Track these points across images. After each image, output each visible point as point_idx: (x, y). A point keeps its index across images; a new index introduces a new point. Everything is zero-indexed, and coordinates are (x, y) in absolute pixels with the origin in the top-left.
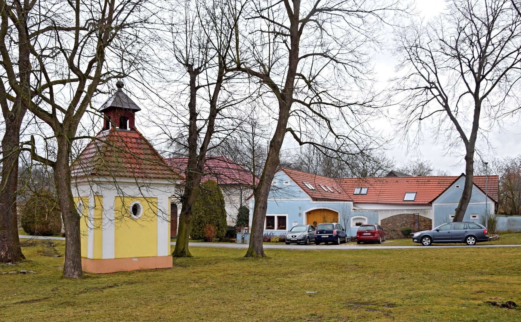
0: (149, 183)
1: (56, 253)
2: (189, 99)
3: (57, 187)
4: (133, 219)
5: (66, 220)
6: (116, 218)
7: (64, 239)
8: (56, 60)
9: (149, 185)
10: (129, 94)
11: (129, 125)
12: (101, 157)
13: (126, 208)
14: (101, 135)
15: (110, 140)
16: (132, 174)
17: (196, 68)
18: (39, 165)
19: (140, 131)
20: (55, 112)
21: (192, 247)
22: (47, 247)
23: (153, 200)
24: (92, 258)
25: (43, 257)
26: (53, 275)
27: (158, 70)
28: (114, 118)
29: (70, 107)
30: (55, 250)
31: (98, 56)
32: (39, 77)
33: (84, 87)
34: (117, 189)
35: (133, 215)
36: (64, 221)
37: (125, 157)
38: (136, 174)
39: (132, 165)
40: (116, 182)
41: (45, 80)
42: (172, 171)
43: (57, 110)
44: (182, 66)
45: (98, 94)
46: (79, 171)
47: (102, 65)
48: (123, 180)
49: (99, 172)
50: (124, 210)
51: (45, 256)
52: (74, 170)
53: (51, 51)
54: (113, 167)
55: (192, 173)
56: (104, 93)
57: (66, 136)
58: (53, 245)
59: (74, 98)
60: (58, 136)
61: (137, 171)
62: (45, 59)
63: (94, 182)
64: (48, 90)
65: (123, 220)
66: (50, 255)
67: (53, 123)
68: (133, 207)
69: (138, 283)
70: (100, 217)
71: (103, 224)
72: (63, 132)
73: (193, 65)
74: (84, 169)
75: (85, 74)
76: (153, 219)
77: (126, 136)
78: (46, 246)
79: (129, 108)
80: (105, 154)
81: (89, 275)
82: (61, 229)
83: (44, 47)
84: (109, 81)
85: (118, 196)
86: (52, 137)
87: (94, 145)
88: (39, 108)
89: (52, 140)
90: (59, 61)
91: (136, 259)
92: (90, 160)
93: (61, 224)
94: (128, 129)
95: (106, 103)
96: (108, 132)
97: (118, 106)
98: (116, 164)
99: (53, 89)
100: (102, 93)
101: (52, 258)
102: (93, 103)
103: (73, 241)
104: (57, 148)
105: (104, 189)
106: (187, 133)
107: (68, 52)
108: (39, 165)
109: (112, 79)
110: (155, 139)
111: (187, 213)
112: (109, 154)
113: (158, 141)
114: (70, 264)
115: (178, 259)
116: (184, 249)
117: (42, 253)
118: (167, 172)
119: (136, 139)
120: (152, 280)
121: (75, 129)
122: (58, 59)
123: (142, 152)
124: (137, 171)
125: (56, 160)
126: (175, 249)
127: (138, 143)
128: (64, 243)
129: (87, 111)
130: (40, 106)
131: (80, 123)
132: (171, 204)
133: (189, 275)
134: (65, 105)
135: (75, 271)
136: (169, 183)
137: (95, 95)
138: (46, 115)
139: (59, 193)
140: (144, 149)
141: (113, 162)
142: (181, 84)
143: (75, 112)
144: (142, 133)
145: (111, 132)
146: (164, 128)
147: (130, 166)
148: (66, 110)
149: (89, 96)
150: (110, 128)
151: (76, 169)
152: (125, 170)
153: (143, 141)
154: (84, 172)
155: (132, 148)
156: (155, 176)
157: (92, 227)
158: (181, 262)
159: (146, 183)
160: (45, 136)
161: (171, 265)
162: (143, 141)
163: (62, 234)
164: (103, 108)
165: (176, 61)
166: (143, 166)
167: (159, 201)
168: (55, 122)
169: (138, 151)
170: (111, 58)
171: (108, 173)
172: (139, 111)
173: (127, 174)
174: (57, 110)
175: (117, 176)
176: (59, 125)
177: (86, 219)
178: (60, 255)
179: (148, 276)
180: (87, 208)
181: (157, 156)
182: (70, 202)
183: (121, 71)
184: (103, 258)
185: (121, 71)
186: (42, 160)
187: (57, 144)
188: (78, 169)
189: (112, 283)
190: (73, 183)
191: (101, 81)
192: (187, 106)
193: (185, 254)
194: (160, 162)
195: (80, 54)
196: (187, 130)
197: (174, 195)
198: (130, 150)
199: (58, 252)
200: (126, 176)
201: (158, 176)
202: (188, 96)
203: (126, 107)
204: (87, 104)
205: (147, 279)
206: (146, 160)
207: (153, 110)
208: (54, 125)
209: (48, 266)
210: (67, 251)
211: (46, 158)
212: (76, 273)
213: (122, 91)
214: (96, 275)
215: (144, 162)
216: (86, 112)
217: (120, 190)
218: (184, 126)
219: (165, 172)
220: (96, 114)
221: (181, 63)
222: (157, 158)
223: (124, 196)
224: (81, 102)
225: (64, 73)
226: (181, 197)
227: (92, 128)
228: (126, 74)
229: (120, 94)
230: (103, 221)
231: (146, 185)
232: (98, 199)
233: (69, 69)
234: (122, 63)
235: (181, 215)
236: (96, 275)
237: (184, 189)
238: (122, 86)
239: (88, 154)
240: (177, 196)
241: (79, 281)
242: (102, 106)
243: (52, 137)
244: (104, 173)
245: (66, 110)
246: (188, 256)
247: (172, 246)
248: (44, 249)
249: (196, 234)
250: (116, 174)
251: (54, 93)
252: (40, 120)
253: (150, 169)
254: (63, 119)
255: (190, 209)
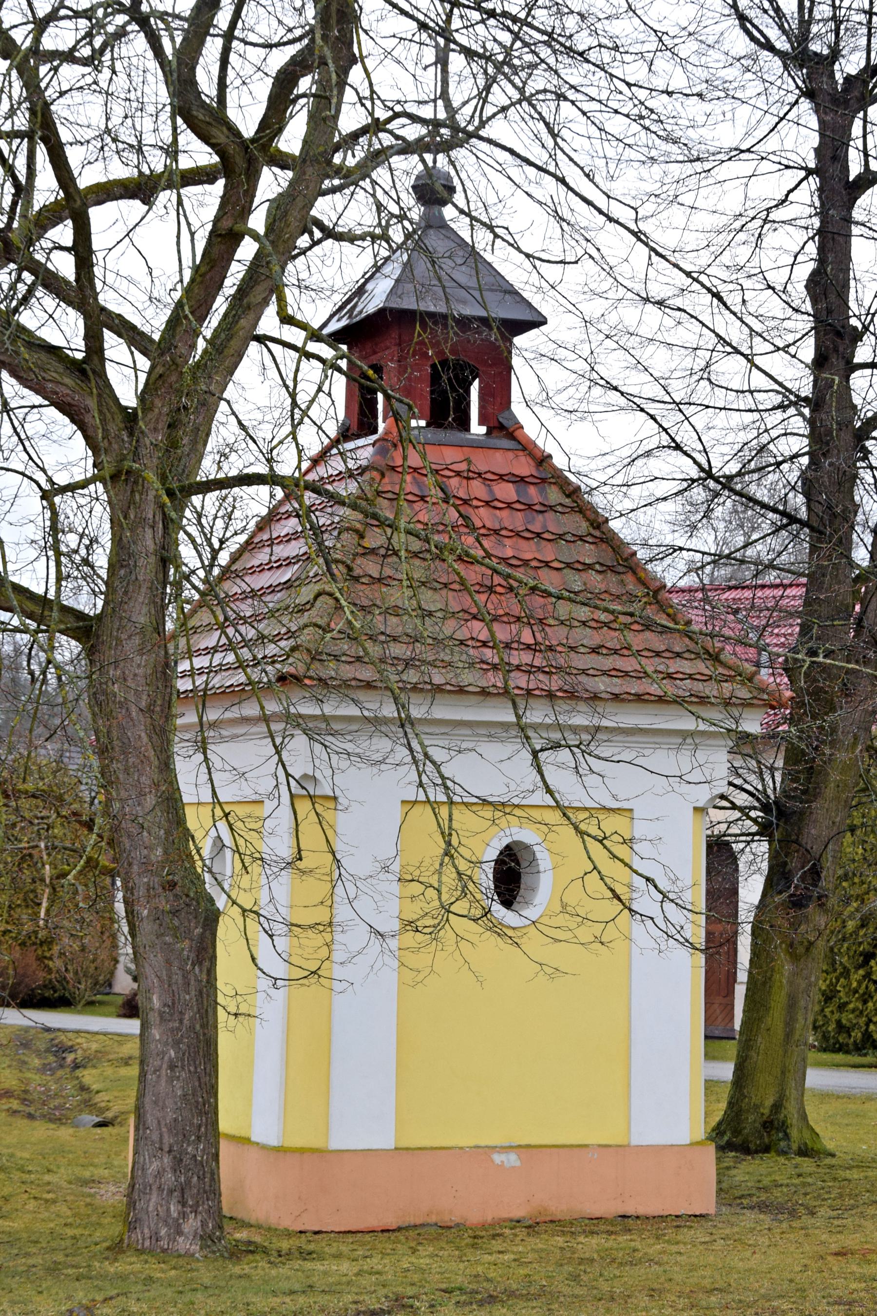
0: (586, 729)
1: (89, 1105)
2: (812, 249)
3: (103, 751)
4: (498, 929)
5: (147, 928)
6: (410, 925)
7: (133, 1026)
8: (106, 73)
9: (586, 737)
10: (482, 239)
11: (482, 408)
12: (332, 588)
13: (463, 866)
14: (336, 465)
15: (379, 493)
16: (495, 680)
17: (854, 72)
18: (16, 630)
19: (540, 443)
20: (101, 350)
21: (825, 1096)
22: (44, 1068)
23: (610, 824)
24: (273, 1142)
25: (22, 1123)
26: (70, 1232)
27: (642, 94)
28: (402, 370)
29: (173, 323)
30: (83, 1088)
31: (324, 37)
32: (21, 165)
33: (246, 211)
34: (415, 761)
35: (498, 910)
36: (133, 932)
37: (462, 582)
38: (519, 680)
39: (496, 626)
40: (412, 722)
41: (54, 184)
42: (715, 658)
43: (110, 338)
44: (773, 65)
45: (315, 243)
46: (218, 658)
47: (342, 83)
48: (443, 711)
49: (317, 670)
50: (449, 877)
51: (31, 1117)
52: (190, 654)
53: (83, 23)
54: (395, 639)
55: (824, 668)
56: (350, 238)
57: (151, 476)
58: (70, 1057)
59: (196, 269)
60: (115, 477)
61: (526, 658)
62: (56, 69)
63: (295, 721)
64: (63, 233)
65: (447, 934)
66: (58, 1119)
67: (88, 411)
68: (499, 862)
69: (527, 1297)
70: (322, 916)
71: (337, 956)
72: (136, 457)
73: (835, 53)
74: (245, 653)
75: (253, 140)
76: (610, 933)
77: (463, 467)
78: (36, 1062)
79: (483, 313)
80: (349, 569)
81: (258, 1239)
82: (112, 973)
83: (49, 9)
84: (381, 174)
85: (422, 797)
86: (84, 484)
87: (294, 521)
88: (23, 329)
89: (82, 501)
90: (121, 81)
91: (512, 1159)
92: (272, 600)
93: (115, 946)
94: (477, 429)
95: (360, 291)
96: (370, 449)
97: (423, 307)
98: (411, 624)
99: (94, 228)
100: (339, 237)
101: (64, 1133)
102: (290, 294)
103: (177, 1043)
104: (106, 539)
105: (344, 764)
106: (799, 444)
107: (168, 28)
108: (16, 630)
109: (396, 161)
110: (619, 480)
111: (798, 903)
112: (372, 567)
113: (635, 491)
114: (159, 1174)
115: (743, 1166)
116: (777, 1107)
117: (15, 1104)
118: (686, 667)
119: (519, 481)
120: (605, 1287)
121: (202, 434)
122: (118, 66)
123: (548, 552)
124: (526, 658)
125: (100, 603)
126: (730, 1104)
127: (530, 506)
128: (132, 1048)
129: (262, 339)
130: (27, 319)
131: (223, 406)
132: (709, 847)
133: (814, 1266)
134: (150, 312)
135: (184, 1215)
136: (702, 727)
137: (304, 252)
138: (54, 364)
139: (111, 783)
140: (561, 536)
141: (395, 611)
142: (766, 166)
143: (201, 344)
144: (550, 448)
145: (384, 446)
146: (670, 419)
147: (484, 636)
148: (156, 337)
149: (274, 259)
150: (381, 426)
151: (199, 653)
152: (458, 657)
153: (554, 495)
154: (241, 665)
155: (496, 532)
156: (617, 686)
157: (278, 969)
158: (766, 1181)
159: (575, 729)
160: (50, 480)
161: (707, 1203)
162: (554, 495)
163: (120, 1000)
164: (344, 322)
165: (740, 44)
166: (557, 635)
167: (640, 830)
168: (100, 404)
169: (529, 551)
170: (390, 43)
171: (367, 673)
172: (534, 332)
173: (467, 678)
174: (110, 338)
175: (415, 688)
176: (119, 418)
177: (252, 924)
178: (109, 1115)
179: (582, 1261)
180: (255, 868)
181: (629, 578)
182: (168, 833)
183: (442, 115)
184: (335, 1144)
185: (442, 115)
186: (30, 606)
187: (107, 517)
188: (215, 650)
189: (382, 1292)
190: (187, 728)
191: (338, 171)
192: (799, 292)
193: (787, 1136)
194: (650, 611)
195: (229, 36)
196: (798, 424)
197: (723, 797)
198: (485, 543)
199: (97, 1099)
200: (461, 691)
201: (635, 687)
202: (803, 236)
203: (468, 311)
204: (266, 302)
205: (575, 1278)
206: (572, 597)
207: (613, 319)
208: (94, 419)
209: (47, 1178)
210: (147, 1100)
211: (51, 595)
212: (192, 1224)
213: (443, 225)
214: (295, 1242)
215: (564, 609)
216: (254, 346)
217: (429, 768)
218: (782, 407)
219: (675, 666)
220: (309, 356)
221: (769, 46)
222: (631, 585)
223: (451, 803)
224: (232, 291)
225: (149, 139)
226: (765, 808)
227: (288, 429)
228: (464, 130)
229: (434, 241)
230: (338, 937)
231: (573, 740)
232: (313, 816)
233: (173, 119)
234: (445, 71)
235: (761, 907)
236: (295, 1242)
237: (780, 763)
238: (445, 194)
239: (261, 569)
240: (742, 799)
241: (205, 1274)
242: (341, 308)
243: (84, 484)
244: (348, 671)
245: (156, 337)
246: (804, 1152)
247: (710, 1085)
248: (28, 1081)
249: (846, 1018)
250: (412, 676)
251: (95, 247)
252: (26, 392)
253: (595, 650)
254: (141, 387)
255: (815, 873)
